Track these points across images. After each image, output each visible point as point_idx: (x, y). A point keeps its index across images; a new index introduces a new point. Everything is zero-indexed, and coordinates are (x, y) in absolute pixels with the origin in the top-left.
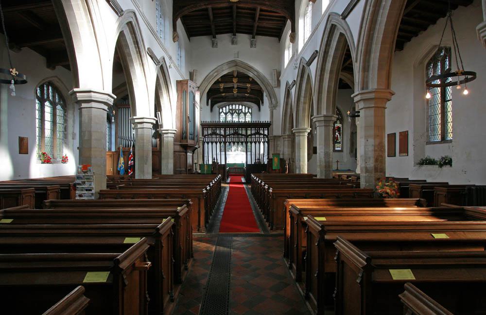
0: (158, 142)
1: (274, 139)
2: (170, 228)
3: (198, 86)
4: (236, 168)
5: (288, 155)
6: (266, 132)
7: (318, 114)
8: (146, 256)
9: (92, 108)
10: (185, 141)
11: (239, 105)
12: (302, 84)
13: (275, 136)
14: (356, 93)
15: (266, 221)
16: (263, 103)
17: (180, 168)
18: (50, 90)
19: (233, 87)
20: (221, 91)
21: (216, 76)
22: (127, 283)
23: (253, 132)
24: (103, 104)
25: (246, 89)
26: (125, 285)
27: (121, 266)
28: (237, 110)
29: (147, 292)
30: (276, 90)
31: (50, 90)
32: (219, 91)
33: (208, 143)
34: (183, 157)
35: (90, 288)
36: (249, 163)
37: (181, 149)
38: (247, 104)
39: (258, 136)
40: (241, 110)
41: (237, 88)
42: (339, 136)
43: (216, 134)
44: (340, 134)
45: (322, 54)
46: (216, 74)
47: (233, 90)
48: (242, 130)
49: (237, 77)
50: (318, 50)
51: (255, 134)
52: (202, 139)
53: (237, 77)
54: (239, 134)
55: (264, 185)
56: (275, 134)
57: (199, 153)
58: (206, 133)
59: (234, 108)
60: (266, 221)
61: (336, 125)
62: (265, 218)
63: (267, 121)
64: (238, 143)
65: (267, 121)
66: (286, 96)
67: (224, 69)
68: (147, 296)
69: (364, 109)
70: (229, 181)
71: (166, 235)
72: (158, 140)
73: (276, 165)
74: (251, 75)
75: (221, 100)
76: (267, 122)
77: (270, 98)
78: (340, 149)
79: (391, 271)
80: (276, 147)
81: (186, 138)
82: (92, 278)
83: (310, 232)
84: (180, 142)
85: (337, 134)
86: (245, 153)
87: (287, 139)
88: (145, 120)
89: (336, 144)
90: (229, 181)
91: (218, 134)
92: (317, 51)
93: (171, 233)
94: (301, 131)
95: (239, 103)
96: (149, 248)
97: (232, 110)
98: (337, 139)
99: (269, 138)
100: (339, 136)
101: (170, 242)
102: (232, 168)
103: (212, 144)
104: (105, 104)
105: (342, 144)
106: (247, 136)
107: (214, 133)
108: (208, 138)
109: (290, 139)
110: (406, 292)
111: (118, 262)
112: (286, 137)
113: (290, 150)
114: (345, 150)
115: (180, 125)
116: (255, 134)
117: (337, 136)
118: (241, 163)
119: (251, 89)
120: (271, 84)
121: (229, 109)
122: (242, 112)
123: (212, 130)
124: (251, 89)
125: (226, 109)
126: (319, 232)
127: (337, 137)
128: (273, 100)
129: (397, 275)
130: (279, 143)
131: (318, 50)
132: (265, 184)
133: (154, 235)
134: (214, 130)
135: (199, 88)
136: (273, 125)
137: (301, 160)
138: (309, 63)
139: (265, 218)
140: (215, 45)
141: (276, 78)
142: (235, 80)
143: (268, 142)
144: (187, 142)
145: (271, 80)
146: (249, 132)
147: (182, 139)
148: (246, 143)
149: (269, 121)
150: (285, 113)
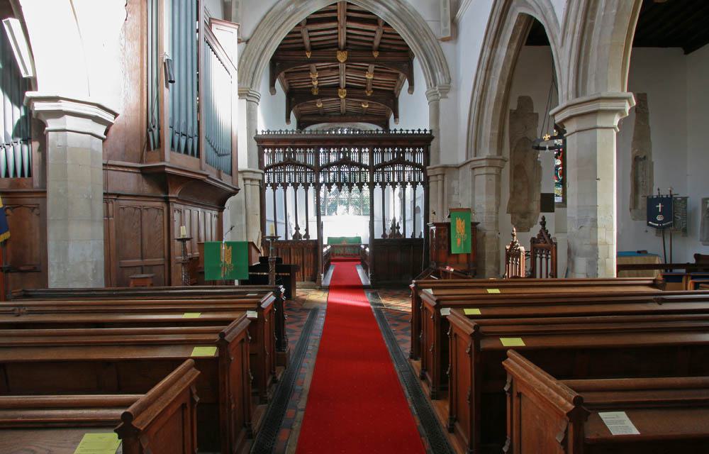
0: (37, 157)
1: (443, 175)
2: (189, 388)
3: (247, 35)
4: (344, 246)
5: (489, 212)
6: (420, 159)
7: (577, 96)
8: (194, 391)
9: (65, 130)
10: (157, 153)
13: (445, 167)
14: (562, 104)
15: (435, 396)
16: (396, 117)
18: (230, 189)
20: (315, 93)
21: (294, 13)
24: (91, 120)
25: (365, 88)
27: (226, 338)
31: (230, 189)
32: (311, 93)
33: (274, 186)
34: (160, 219)
35: (199, 361)
36: (378, 236)
37: (146, 188)
41: (347, 87)
47: (338, 93)
51: (392, 164)
56: (445, 160)
57: (250, 213)
58: (267, 161)
60: (435, 396)
63: (422, 129)
64: (350, 185)
65: (422, 129)
68: (250, 374)
69: (576, 134)
70: (327, 280)
71: (268, 310)
72: (36, 145)
73: (460, 243)
77: (431, 68)
79: (602, 415)
80: (446, 194)
81: (160, 144)
82: (199, 352)
83: (456, 335)
84: (141, 162)
87: (484, 171)
88: (65, 106)
90: (327, 280)
93: (192, 401)
94: (603, 105)
96: (199, 375)
102: (336, 246)
104: (94, 120)
108: (274, 173)
109: (493, 170)
110: (508, 359)
112: (484, 163)
113: (493, 198)
115: (138, 100)
118: (355, 236)
120: (435, 33)
123: (285, 153)
128: (439, 74)
129: (506, 342)
130: (455, 183)
134: (290, 154)
135: (247, 42)
136: (439, 138)
137: (599, 222)
143: (426, 184)
144: (163, 159)
146: (378, 160)
147: (149, 149)
149: (428, 129)
150: (481, 96)
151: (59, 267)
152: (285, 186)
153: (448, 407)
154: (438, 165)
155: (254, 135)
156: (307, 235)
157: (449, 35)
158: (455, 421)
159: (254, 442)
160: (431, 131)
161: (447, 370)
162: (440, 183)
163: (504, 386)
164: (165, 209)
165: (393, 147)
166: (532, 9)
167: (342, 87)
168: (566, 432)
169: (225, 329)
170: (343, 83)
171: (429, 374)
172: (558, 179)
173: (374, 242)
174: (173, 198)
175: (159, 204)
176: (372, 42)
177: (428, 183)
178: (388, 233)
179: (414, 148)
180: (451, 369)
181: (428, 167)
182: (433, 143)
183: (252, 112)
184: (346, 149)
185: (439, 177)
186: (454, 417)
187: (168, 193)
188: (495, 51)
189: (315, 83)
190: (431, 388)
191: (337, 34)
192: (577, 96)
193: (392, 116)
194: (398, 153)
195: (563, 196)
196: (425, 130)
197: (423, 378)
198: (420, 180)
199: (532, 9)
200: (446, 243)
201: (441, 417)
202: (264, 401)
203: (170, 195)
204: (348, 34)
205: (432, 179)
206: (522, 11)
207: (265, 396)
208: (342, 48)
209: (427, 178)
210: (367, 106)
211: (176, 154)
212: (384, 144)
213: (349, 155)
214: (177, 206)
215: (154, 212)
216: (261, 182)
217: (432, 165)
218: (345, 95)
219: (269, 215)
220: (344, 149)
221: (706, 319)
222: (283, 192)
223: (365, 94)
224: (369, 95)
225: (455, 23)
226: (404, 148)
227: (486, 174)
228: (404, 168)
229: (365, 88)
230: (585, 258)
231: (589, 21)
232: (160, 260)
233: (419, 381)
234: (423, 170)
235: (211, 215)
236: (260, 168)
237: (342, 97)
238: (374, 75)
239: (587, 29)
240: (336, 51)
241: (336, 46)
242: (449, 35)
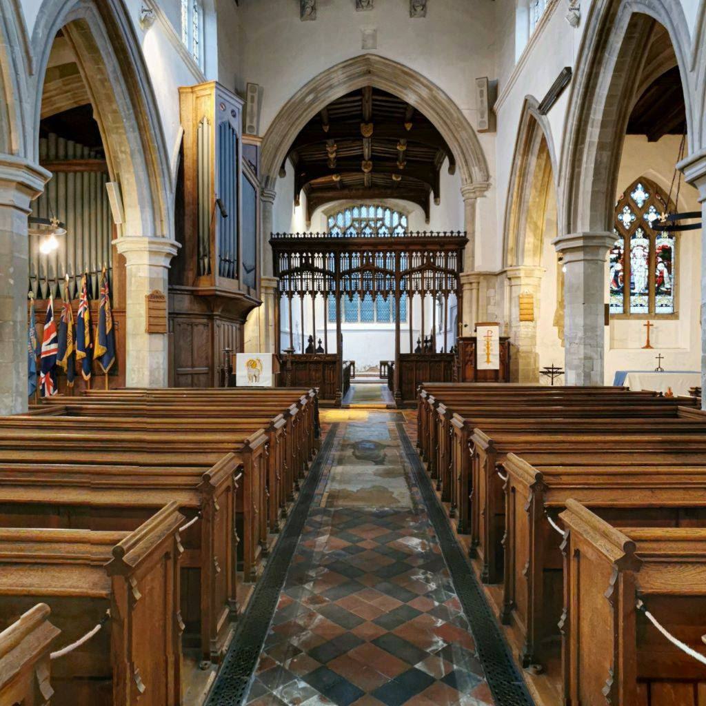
6: (453, 264)
7: (569, 232)
11: (377, 207)
12: (594, 88)
13: (479, 274)
16: (437, 196)
17: (193, 366)
19: (361, 157)
20: (332, 166)
22: (138, 596)
23: (416, 263)
26: (135, 601)
27: (212, 481)
28: (373, 220)
29: (179, 612)
30: (484, 139)
36: (405, 349)
38: (397, 205)
39: (431, 275)
40: (382, 219)
41: (373, 158)
42: (666, 274)
43: (313, 270)
44: (669, 267)
45: (581, 79)
46: (311, 97)
47: (361, 166)
48: (385, 257)
49: (371, 120)
50: (573, 65)
51: (421, 270)
52: (274, 284)
53: (371, 120)
54: (378, 270)
55: (427, 398)
58: (284, 265)
59: (364, 215)
61: (657, 241)
62: (438, 489)
66: (524, 136)
67: (335, 81)
68: (180, 619)
74: (411, 99)
75: (330, 194)
76: (455, 234)
78: (669, 310)
83: (577, 553)
85: (661, 267)
86: (685, 233)
89: (658, 298)
91: (317, 270)
92: (568, 69)
93: (176, 549)
95: (376, 201)
97: (360, 221)
98: (662, 283)
99: (463, 280)
100: (666, 274)
101: (262, 470)
103: (302, 297)
105: (676, 297)
106: (399, 275)
107: (307, 267)
111: (249, 442)
114: (684, 311)
116: (421, 270)
117: (661, 273)
119: (409, 161)
121: (354, 220)
122: (383, 225)
124: (409, 161)
125: (344, 218)
126: (531, 487)
127: (662, 277)
131: (573, 65)
132: (428, 395)
133: (204, 486)
136: (474, 241)
138: (545, 107)
139: (429, 469)
140: (309, 10)
141: (486, 104)
142: (367, 131)
145: (468, 105)
148: (398, 294)
151: (139, 371)
152: (302, 294)
153: (503, 592)
154: (473, 273)
155: (269, 239)
156: (292, 350)
157: (486, 127)
158: (511, 609)
159: (219, 667)
160: (465, 233)
161: (502, 538)
162: (475, 292)
163: (560, 544)
164: (210, 325)
165: (422, 252)
166: (653, 9)
167: (366, 158)
168: (616, 586)
169: (208, 471)
170: (367, 152)
171: (521, 615)
172: (618, 286)
173: (401, 357)
174: (216, 315)
175: (205, 321)
176: (404, 113)
177: (462, 292)
178: (414, 352)
179: (447, 252)
180: (508, 539)
181: (461, 274)
182: (468, 246)
183: (267, 214)
184: (370, 254)
185: (474, 285)
186: (509, 605)
187: (213, 311)
188: (527, 159)
189: (332, 156)
190: (483, 568)
191: (361, 105)
192: (569, 232)
193: (432, 195)
194: (428, 258)
195: (624, 306)
196: (459, 232)
197: (507, 620)
198: (452, 288)
199: (653, 9)
200: (472, 357)
201: (492, 601)
202: (250, 578)
203: (215, 313)
204: (373, 105)
205: (466, 287)
206: (636, 10)
207: (252, 570)
208: (367, 119)
209: (460, 286)
210: (399, 179)
211: (222, 278)
212: (411, 248)
213: (373, 260)
214: (218, 322)
215: (201, 327)
216: (277, 289)
217: (467, 270)
218: (370, 168)
219: (285, 327)
220: (368, 254)
221: (701, 431)
222: (300, 301)
223: (397, 166)
224: (401, 167)
225: (492, 114)
226: (434, 252)
227: (584, 260)
228: (434, 275)
229: (396, 159)
230: (574, 371)
231: (576, 170)
232: (204, 369)
233: (498, 625)
234: (457, 277)
235: (236, 326)
236: (275, 275)
237: (366, 170)
238: (407, 146)
239: (575, 176)
240: (359, 123)
241: (360, 117)
242: (486, 127)
